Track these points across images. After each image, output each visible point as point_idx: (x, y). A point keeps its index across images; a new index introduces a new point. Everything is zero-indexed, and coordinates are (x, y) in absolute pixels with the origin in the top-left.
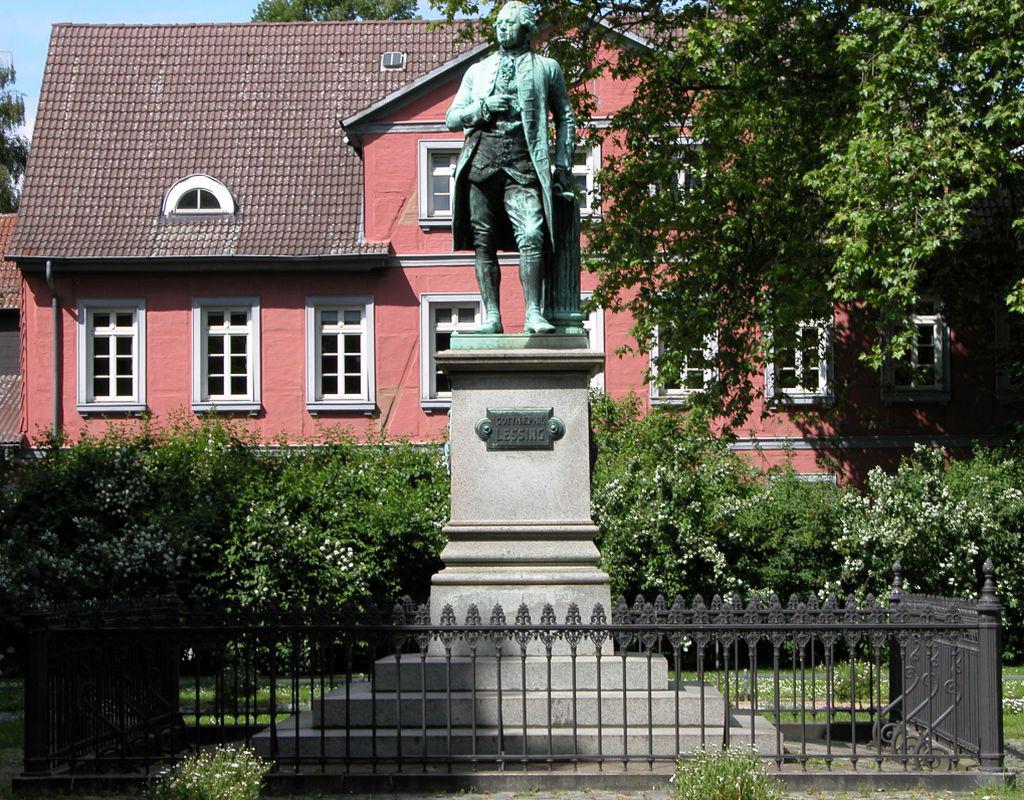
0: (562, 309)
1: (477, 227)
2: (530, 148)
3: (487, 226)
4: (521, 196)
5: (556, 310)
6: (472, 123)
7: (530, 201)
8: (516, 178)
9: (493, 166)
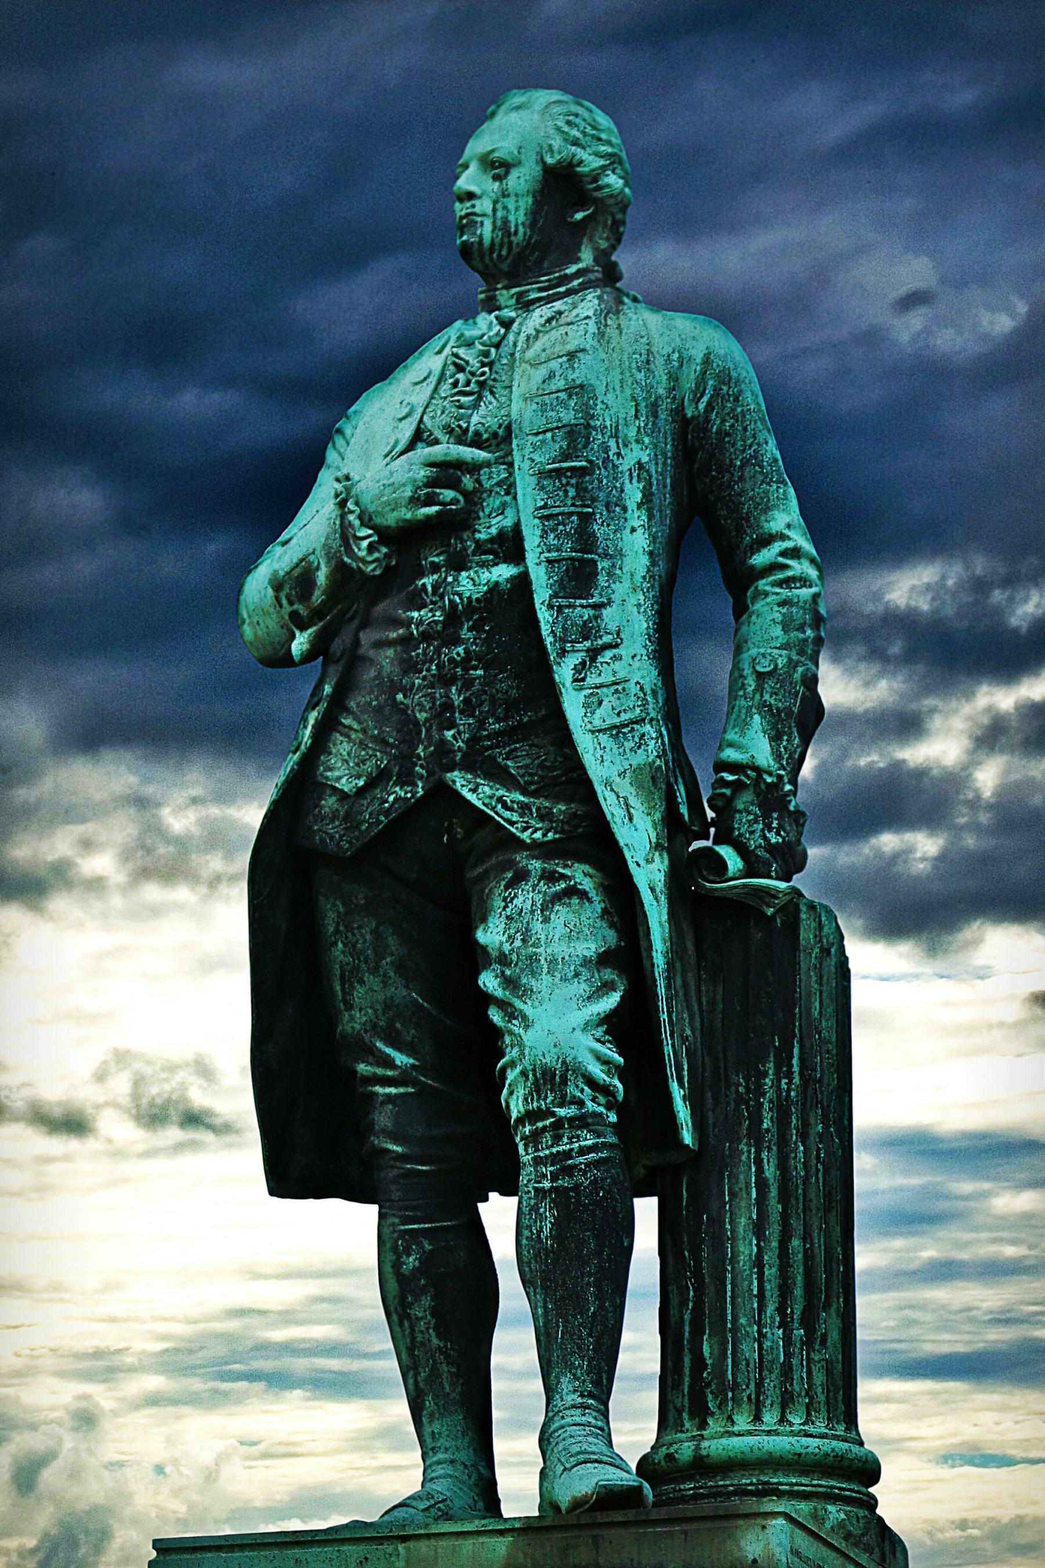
0: (742, 1422)
1: (362, 1068)
2: (564, 673)
3: (401, 1059)
4: (525, 898)
5: (714, 1425)
6: (318, 597)
7: (561, 915)
8: (501, 816)
9: (407, 779)
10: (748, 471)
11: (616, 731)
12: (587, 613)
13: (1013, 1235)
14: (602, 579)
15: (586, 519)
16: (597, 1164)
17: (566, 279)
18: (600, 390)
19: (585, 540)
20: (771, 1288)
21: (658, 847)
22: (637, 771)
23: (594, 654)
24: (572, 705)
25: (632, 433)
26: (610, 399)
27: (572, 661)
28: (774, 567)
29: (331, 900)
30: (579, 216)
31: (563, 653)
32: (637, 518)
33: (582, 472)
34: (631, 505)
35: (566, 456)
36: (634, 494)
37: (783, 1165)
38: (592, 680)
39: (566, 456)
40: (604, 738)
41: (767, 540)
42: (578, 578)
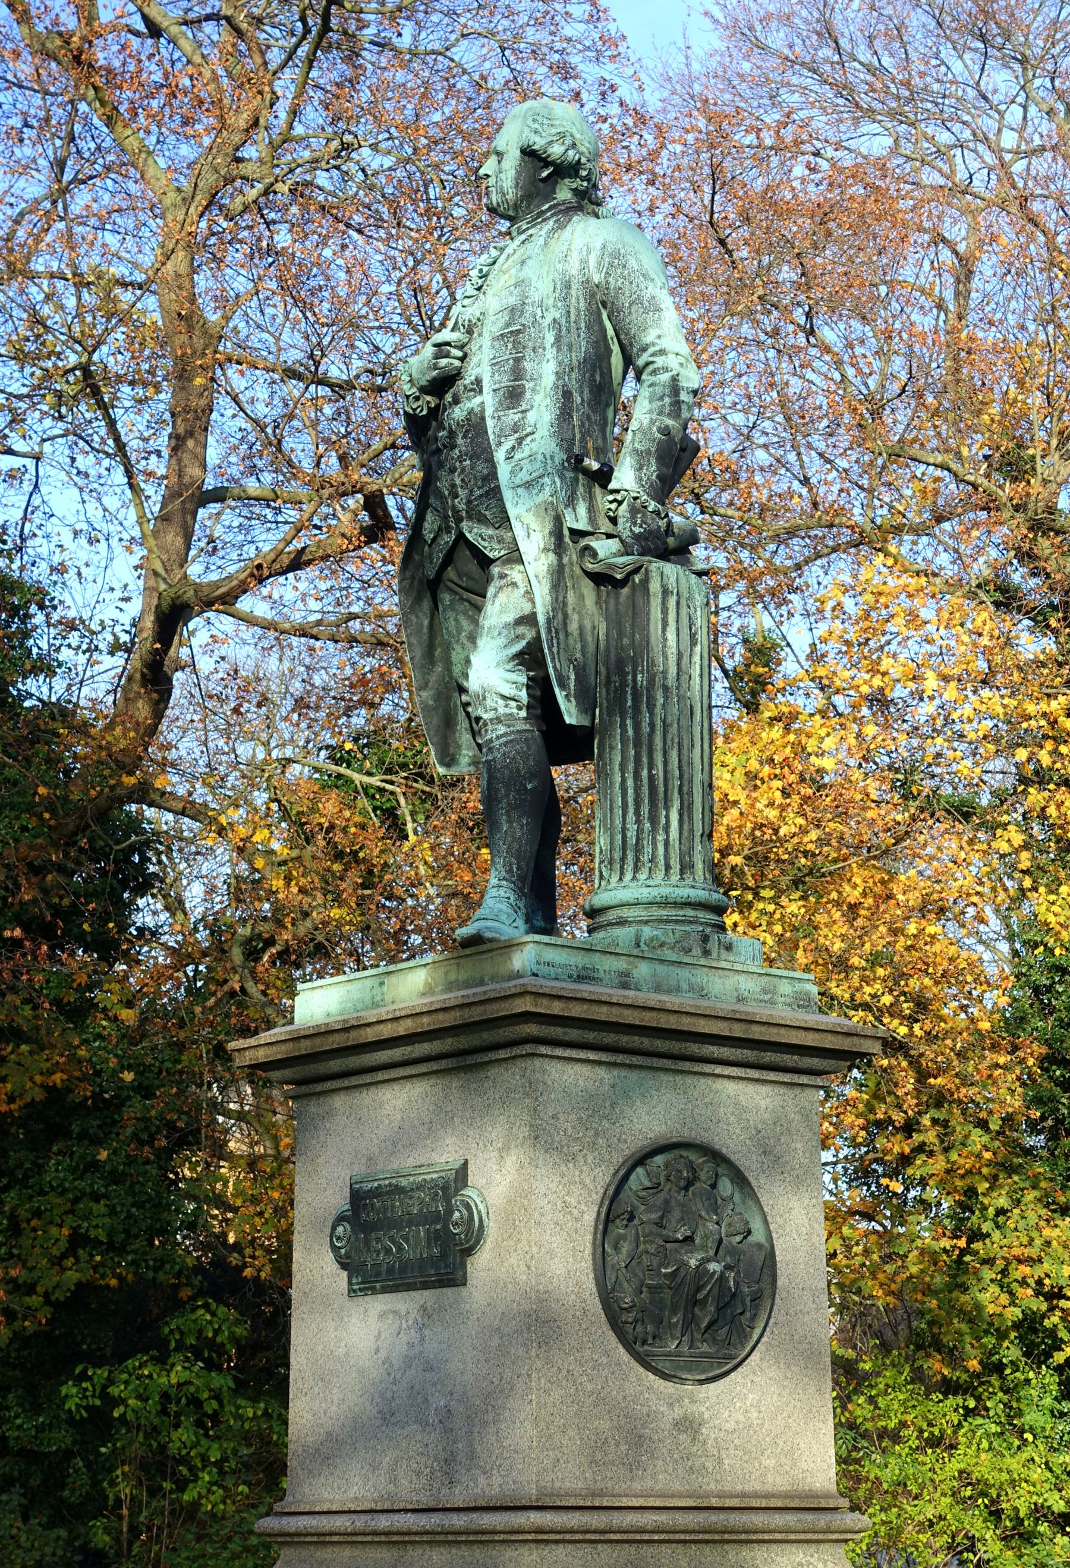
2: (500, 456)
10: (634, 308)
11: (528, 485)
12: (517, 417)
13: (661, 805)
14: (528, 395)
15: (518, 361)
16: (506, 744)
17: (543, 212)
18: (534, 279)
19: (517, 373)
20: (630, 800)
21: (546, 550)
22: (538, 507)
23: (520, 441)
24: (504, 471)
25: (551, 302)
26: (539, 285)
27: (507, 445)
28: (648, 364)
29: (54, 699)
30: (545, 174)
31: (500, 444)
32: (551, 353)
33: (518, 332)
34: (548, 345)
35: (508, 325)
36: (550, 338)
37: (637, 727)
38: (518, 456)
39: (508, 325)
40: (520, 491)
41: (644, 349)
42: (513, 396)
